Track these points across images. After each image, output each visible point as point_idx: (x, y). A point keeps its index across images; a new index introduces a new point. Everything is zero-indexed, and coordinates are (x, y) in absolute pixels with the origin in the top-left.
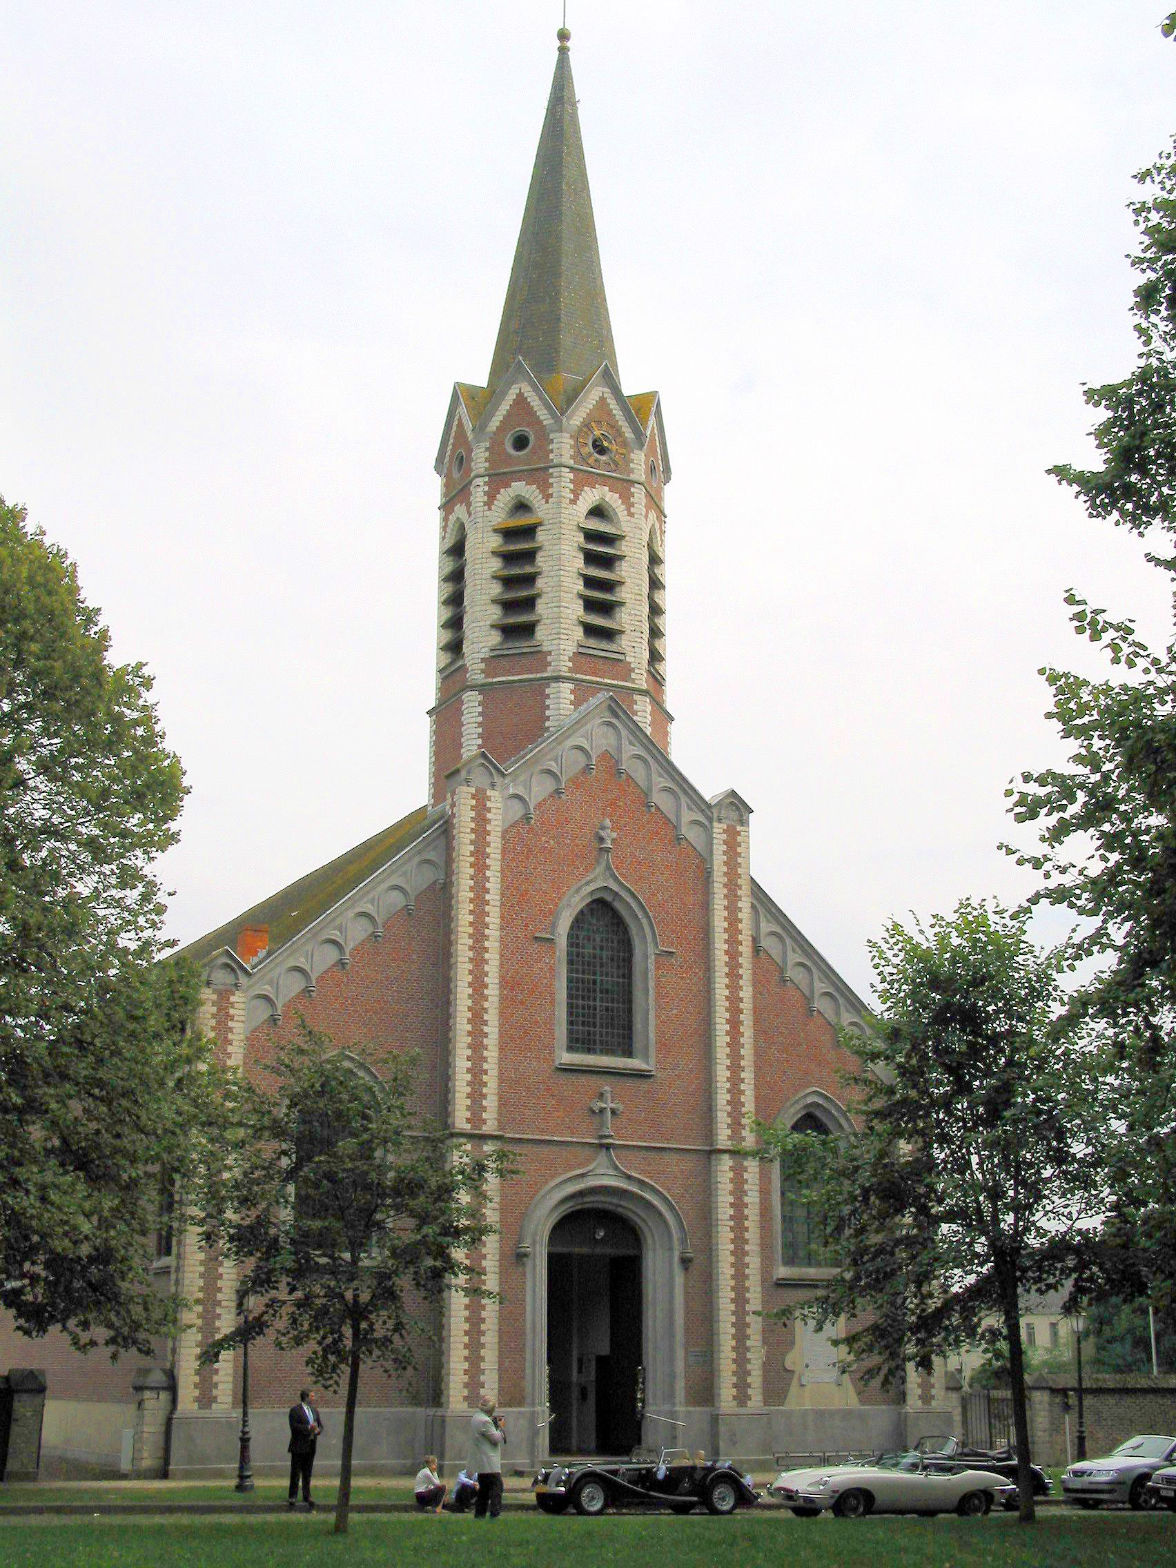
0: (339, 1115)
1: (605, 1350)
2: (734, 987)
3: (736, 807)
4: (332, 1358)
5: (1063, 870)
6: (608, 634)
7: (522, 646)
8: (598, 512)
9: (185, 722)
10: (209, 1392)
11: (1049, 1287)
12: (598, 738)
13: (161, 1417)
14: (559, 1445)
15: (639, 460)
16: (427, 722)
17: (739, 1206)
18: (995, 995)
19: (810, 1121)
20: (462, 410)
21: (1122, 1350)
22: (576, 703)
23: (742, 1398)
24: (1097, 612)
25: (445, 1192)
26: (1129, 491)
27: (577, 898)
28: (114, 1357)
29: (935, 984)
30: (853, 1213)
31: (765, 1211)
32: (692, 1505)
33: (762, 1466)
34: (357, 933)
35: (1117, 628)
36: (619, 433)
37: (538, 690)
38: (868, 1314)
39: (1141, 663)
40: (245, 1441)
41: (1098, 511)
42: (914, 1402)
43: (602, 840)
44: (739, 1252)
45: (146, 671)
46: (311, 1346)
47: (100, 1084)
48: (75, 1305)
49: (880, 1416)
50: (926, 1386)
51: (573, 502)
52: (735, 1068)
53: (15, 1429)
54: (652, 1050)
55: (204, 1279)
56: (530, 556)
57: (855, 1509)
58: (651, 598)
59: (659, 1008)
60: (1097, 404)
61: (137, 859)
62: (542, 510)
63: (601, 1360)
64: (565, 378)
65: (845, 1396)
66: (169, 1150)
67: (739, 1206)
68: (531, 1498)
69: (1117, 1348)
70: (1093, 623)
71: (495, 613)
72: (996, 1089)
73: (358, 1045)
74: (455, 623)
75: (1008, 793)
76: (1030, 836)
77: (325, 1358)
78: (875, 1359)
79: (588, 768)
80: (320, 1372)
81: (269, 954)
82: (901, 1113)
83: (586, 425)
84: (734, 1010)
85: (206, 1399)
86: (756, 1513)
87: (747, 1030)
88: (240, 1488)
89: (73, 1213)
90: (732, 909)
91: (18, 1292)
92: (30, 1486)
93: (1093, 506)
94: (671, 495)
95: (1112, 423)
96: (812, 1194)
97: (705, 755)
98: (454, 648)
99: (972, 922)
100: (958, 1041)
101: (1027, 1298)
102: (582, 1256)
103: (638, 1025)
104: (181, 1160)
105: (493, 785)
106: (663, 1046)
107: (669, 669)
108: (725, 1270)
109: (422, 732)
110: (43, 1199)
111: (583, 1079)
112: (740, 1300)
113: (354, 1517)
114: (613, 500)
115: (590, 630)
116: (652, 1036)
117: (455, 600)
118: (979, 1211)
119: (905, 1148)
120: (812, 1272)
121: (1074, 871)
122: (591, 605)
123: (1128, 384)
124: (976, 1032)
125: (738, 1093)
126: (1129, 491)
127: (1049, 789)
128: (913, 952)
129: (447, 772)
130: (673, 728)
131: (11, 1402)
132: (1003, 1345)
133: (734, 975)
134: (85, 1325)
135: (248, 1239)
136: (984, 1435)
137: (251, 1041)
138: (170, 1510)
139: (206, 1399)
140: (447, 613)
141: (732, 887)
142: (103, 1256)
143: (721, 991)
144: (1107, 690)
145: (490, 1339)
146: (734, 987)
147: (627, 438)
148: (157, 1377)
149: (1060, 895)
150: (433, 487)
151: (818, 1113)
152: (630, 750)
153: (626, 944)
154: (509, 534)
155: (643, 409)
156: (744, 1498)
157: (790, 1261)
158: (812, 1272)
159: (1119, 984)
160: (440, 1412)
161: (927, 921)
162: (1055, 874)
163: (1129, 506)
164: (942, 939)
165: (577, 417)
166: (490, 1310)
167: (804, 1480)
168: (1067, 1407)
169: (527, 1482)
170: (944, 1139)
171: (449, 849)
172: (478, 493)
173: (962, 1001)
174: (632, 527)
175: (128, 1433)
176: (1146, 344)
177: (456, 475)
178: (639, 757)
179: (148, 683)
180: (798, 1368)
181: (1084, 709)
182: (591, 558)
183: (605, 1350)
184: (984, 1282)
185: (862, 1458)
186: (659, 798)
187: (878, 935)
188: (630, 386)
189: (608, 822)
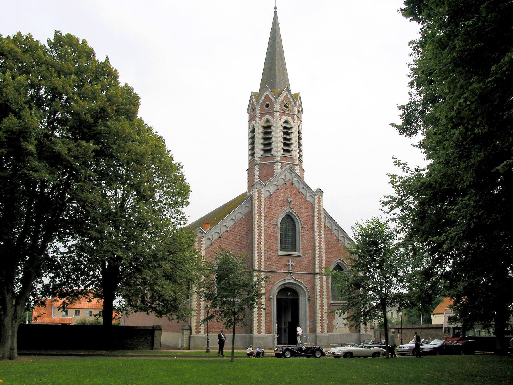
0: (230, 269)
1: (290, 320)
2: (320, 235)
3: (320, 192)
4: (229, 323)
5: (394, 214)
6: (289, 151)
7: (269, 154)
8: (286, 122)
9: (190, 175)
10: (199, 331)
11: (393, 306)
12: (287, 176)
13: (188, 336)
14: (279, 343)
15: (296, 109)
16: (246, 172)
17: (321, 287)
18: (381, 238)
19: (339, 267)
20: (253, 98)
21: (414, 319)
22: (282, 168)
23: (322, 331)
24: (399, 161)
25: (253, 286)
26: (408, 129)
27: (282, 215)
28: (178, 322)
29: (367, 236)
30: (348, 289)
31: (328, 288)
32: (311, 356)
33: (327, 347)
34: (231, 224)
35: (404, 164)
36: (291, 103)
37: (272, 165)
38: (351, 313)
39: (409, 172)
40: (208, 341)
41: (401, 133)
42: (362, 332)
43: (288, 201)
44: (322, 297)
45: (181, 164)
46: (224, 321)
47: (174, 261)
48: (169, 311)
49: (355, 335)
50: (366, 328)
51: (280, 120)
52: (320, 254)
53: (155, 338)
54: (301, 251)
55: (198, 305)
56: (270, 133)
57: (348, 357)
58: (299, 142)
59: (302, 240)
60: (400, 109)
61: (180, 208)
62: (273, 122)
63: (289, 322)
64: (278, 90)
65: (346, 331)
66: (189, 276)
67: (321, 287)
68: (274, 354)
69: (413, 318)
70: (399, 163)
71: (262, 147)
72: (381, 261)
73: (232, 250)
74: (252, 149)
75: (380, 201)
76: (387, 209)
77: (228, 323)
78: (353, 323)
79: (285, 183)
80: (227, 326)
81: (210, 229)
82: (360, 266)
83: (283, 101)
84: (320, 241)
85: (198, 332)
86: (326, 357)
87: (323, 245)
88: (207, 352)
89: (167, 289)
90: (319, 216)
91: (155, 308)
92: (159, 351)
93: (400, 132)
94: (303, 117)
95: (404, 114)
96: (338, 285)
97: (312, 179)
98: (252, 155)
99: (376, 222)
100: (372, 248)
101: (388, 308)
102: (284, 299)
103: (297, 245)
104: (192, 278)
105: (262, 188)
106: (304, 249)
107: (303, 159)
108: (318, 302)
109: (245, 174)
110: (163, 287)
111: (285, 257)
112: (322, 309)
113: (234, 359)
114: (290, 119)
115: (285, 150)
116: (301, 247)
117: (252, 144)
118: (377, 288)
119: (361, 274)
120: (339, 302)
121: (396, 215)
122: (285, 144)
123: (407, 105)
124: (377, 247)
125: (321, 260)
126: (408, 129)
127: (389, 199)
128: (362, 229)
129: (251, 185)
130: (304, 173)
131: (154, 332)
132: (383, 320)
133: (320, 231)
134: (171, 315)
135: (209, 297)
136: (380, 339)
137: (207, 249)
138: (192, 357)
139: (198, 332)
140: (250, 147)
141: (319, 211)
142: (175, 300)
143: (317, 236)
144: (401, 178)
145: (263, 318)
146: (320, 235)
147: (293, 104)
148: (187, 327)
149: (394, 220)
150: (247, 116)
151: (340, 265)
152: (295, 179)
153: (294, 225)
154: (265, 128)
155: (296, 97)
156: (323, 354)
157: (333, 299)
158: (339, 302)
159: (407, 240)
160: (252, 335)
161: (365, 222)
162: (392, 215)
163: (408, 132)
164: (369, 225)
165: (280, 100)
166: (263, 312)
167: (337, 350)
168: (399, 332)
169: (273, 351)
170: (369, 272)
171: (252, 203)
172: (258, 117)
173: (372, 241)
174: (294, 125)
175: (180, 340)
176: (411, 96)
177: (252, 113)
178: (297, 181)
179: (182, 167)
180: (336, 324)
181: (396, 182)
182: (285, 133)
183: (290, 320)
184: (378, 305)
185: (350, 345)
186: (302, 191)
187: (354, 225)
188: (293, 92)
189: (290, 196)
